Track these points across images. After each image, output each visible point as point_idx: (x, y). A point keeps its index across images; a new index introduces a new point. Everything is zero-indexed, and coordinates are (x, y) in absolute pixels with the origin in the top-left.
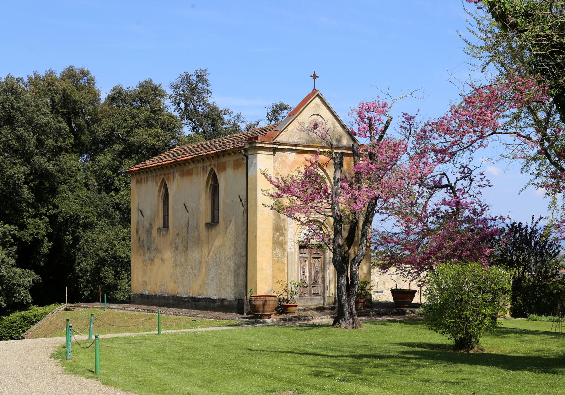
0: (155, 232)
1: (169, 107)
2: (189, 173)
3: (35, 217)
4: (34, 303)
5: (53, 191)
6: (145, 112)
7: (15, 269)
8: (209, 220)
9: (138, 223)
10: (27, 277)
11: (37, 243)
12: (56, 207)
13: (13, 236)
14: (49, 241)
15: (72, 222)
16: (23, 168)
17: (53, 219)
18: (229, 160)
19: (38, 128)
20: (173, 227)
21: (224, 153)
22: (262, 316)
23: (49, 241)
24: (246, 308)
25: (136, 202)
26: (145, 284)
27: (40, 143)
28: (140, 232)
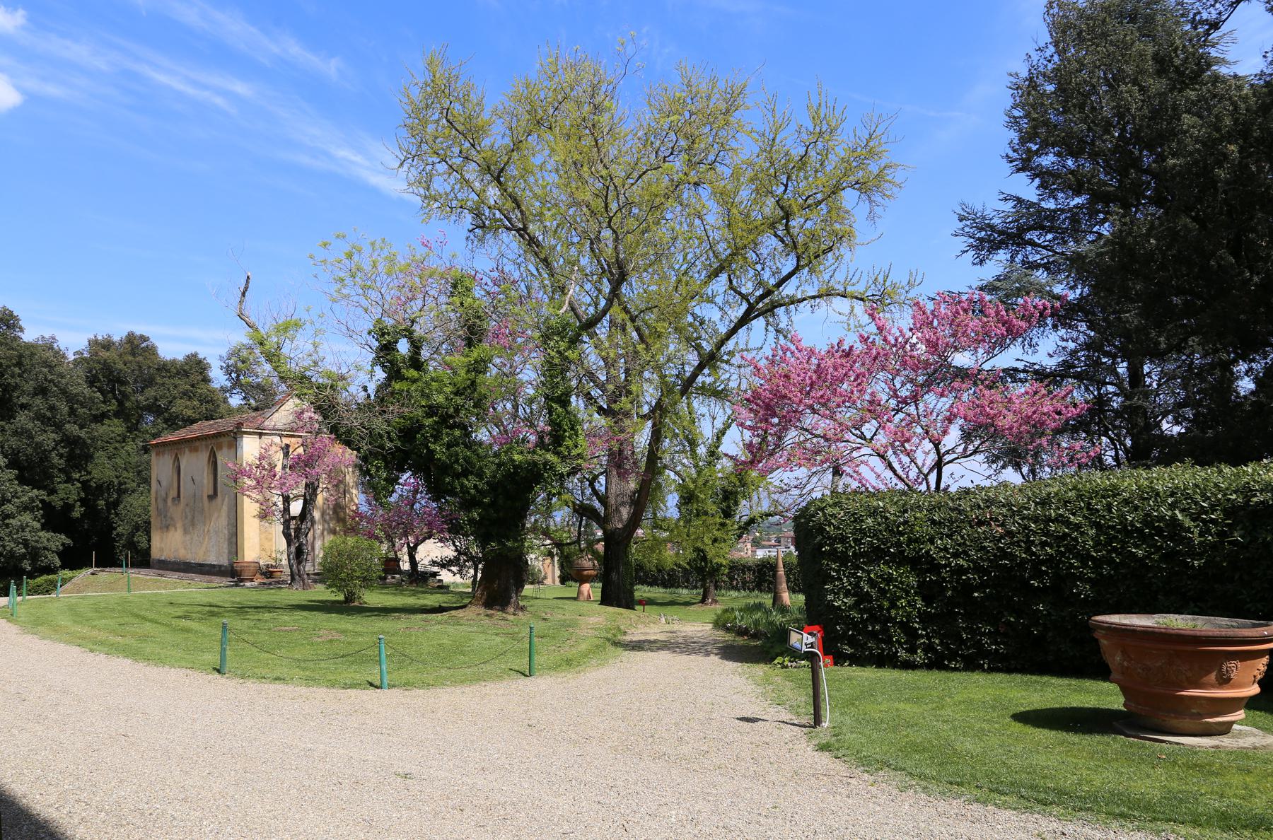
1: (218, 378)
2: (196, 450)
3: (66, 482)
4: (63, 567)
5: (89, 458)
6: (183, 385)
7: (42, 534)
8: (211, 492)
10: (55, 541)
11: (68, 507)
12: (89, 473)
13: (42, 501)
14: (81, 506)
15: (101, 489)
16: (54, 435)
17: (85, 485)
18: (224, 440)
19: (71, 398)
21: (219, 435)
22: (242, 580)
23: (81, 506)
24: (233, 573)
26: (162, 550)
27: (72, 412)
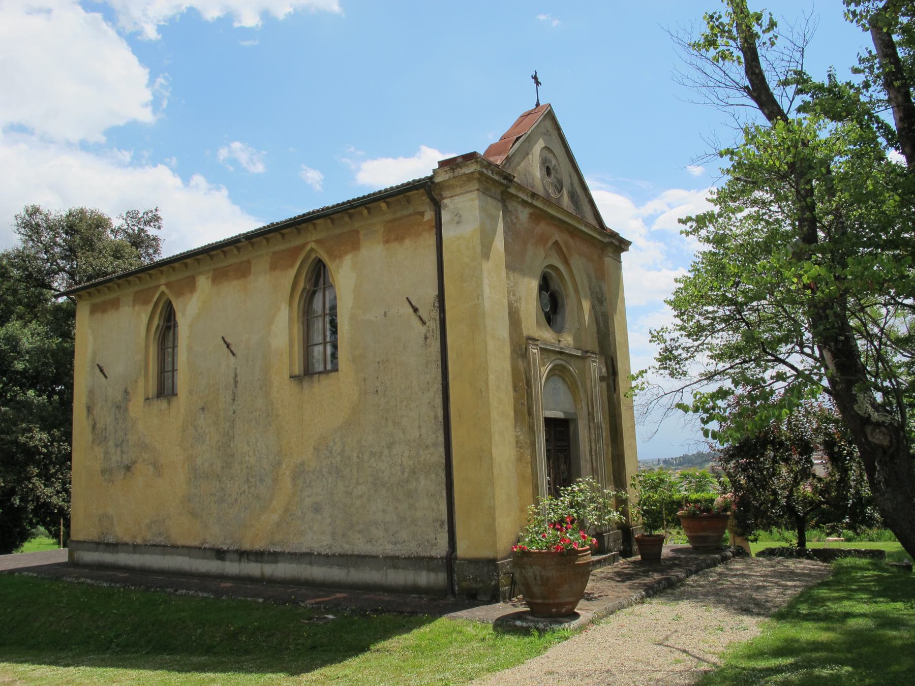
0: (136, 407)
8: (298, 369)
9: (91, 393)
20: (191, 392)
25: (90, 350)
28: (97, 410)
